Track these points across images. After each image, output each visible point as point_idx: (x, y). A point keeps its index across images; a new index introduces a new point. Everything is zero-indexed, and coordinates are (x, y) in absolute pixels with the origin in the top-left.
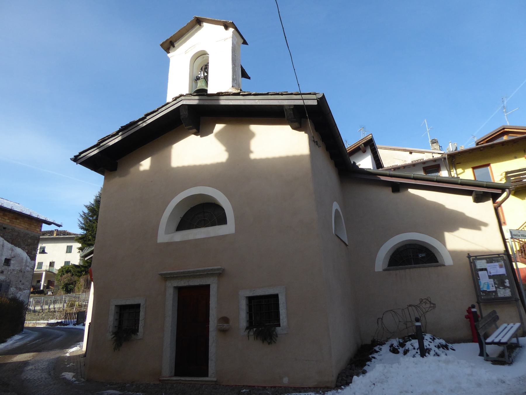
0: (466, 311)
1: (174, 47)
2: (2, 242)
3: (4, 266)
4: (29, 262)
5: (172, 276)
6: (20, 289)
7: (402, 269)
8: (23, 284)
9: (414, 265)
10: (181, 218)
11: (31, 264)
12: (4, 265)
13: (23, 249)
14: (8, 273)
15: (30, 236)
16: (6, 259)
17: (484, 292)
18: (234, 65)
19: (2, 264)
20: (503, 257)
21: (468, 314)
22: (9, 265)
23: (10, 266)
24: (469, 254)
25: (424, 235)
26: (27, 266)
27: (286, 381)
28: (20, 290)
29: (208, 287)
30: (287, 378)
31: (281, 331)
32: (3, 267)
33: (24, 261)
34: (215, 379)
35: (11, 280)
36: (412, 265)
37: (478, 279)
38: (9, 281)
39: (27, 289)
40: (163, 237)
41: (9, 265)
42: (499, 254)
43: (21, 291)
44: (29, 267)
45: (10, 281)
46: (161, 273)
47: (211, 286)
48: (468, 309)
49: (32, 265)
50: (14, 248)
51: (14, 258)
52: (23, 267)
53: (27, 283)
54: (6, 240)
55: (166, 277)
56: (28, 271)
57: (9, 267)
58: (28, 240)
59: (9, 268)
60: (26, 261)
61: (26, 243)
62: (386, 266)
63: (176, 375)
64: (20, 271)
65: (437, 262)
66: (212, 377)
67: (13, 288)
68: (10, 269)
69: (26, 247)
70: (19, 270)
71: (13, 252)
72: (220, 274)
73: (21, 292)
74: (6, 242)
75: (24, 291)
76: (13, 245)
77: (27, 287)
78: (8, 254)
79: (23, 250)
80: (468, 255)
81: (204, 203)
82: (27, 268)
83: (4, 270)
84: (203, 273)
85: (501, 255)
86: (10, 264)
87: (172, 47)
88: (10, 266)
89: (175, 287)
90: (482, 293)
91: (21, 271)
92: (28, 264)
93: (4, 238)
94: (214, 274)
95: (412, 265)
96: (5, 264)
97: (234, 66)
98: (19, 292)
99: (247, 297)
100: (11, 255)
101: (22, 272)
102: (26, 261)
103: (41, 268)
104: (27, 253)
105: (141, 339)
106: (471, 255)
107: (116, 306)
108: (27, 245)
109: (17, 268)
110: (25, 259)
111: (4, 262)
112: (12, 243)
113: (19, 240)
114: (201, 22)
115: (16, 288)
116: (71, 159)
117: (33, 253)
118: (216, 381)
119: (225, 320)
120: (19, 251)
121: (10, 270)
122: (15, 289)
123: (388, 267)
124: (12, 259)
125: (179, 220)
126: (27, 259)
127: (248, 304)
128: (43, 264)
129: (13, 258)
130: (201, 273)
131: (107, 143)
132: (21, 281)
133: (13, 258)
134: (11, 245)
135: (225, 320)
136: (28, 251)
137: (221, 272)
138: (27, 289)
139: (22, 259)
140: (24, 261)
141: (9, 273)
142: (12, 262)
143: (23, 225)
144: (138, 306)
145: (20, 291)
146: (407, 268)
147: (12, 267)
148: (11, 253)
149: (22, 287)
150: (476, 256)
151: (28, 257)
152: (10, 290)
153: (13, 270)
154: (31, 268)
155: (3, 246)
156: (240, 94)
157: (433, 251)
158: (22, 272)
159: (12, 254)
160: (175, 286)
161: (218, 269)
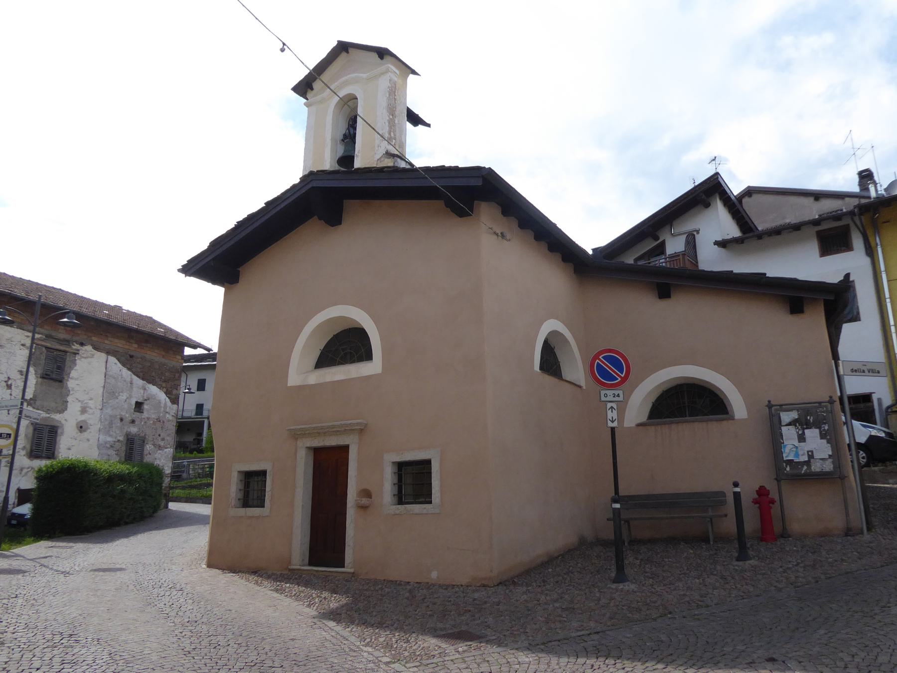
0: (755, 492)
1: (312, 89)
2: (130, 377)
3: (135, 413)
4: (170, 407)
5: (303, 433)
6: (160, 447)
7: (702, 421)
8: (163, 439)
9: (690, 416)
10: (320, 350)
11: (172, 409)
12: (135, 411)
13: (160, 387)
14: (141, 423)
15: (168, 368)
16: (137, 403)
17: (790, 462)
18: (392, 115)
19: (133, 410)
20: (826, 406)
21: (757, 497)
22: (141, 411)
23: (142, 412)
24: (769, 402)
25: (696, 367)
26: (167, 413)
27: (434, 575)
28: (160, 448)
29: (345, 449)
30: (436, 572)
31: (433, 509)
32: (134, 414)
33: (162, 405)
34: (352, 570)
35: (147, 434)
36: (686, 417)
37: (780, 441)
38: (143, 435)
39: (169, 446)
40: (294, 379)
41: (141, 411)
42: (820, 403)
43: (161, 450)
44: (169, 414)
45: (145, 435)
46: (289, 428)
47: (350, 447)
48: (759, 489)
49: (174, 411)
50: (146, 386)
51: (148, 401)
52: (162, 415)
53: (168, 438)
54: (134, 373)
55: (296, 435)
56: (169, 421)
57: (142, 414)
58: (166, 374)
59: (142, 415)
60: (165, 405)
61: (163, 378)
62: (644, 418)
63: (310, 564)
64: (157, 420)
65: (727, 413)
66: (348, 569)
67: (150, 446)
68: (143, 417)
69: (164, 385)
70: (156, 418)
71: (146, 392)
72: (362, 431)
73: (160, 451)
74: (135, 377)
75: (166, 450)
76: (145, 382)
77: (169, 444)
78: (140, 395)
79: (160, 388)
80: (767, 403)
81: (349, 328)
82: (168, 416)
83: (135, 419)
84: (340, 429)
85: (823, 404)
86: (143, 410)
87: (309, 90)
88: (142, 412)
89: (309, 448)
90: (784, 464)
91: (159, 420)
92: (168, 410)
93: (132, 372)
94: (353, 430)
95: (686, 418)
96: (137, 409)
97: (391, 117)
98: (159, 452)
99: (394, 463)
100: (143, 397)
101: (160, 421)
102: (165, 405)
103: (202, 414)
104: (166, 393)
105: (267, 516)
106: (773, 403)
107: (239, 472)
108: (165, 381)
109: (153, 416)
110: (163, 402)
111: (134, 406)
112: (143, 379)
113: (153, 374)
114: (349, 48)
115: (154, 445)
116: (179, 270)
117: (174, 393)
118: (354, 573)
119: (366, 493)
120: (153, 389)
121: (144, 418)
122: (153, 447)
123: (647, 419)
124: (145, 402)
125: (318, 353)
126: (165, 401)
127: (397, 471)
128: (205, 407)
129: (146, 400)
130: (338, 429)
131: (306, 185)
132: (159, 435)
133: (146, 400)
134: (141, 381)
135: (366, 493)
136: (167, 390)
137: (363, 428)
138: (169, 446)
139: (160, 402)
140: (162, 405)
141: (142, 423)
142: (145, 407)
143: (156, 351)
144: (263, 473)
145: (159, 449)
146: (672, 423)
147: (145, 415)
148: (144, 393)
149: (162, 443)
150: (781, 406)
151: (168, 400)
152: (145, 448)
153: (148, 418)
154: (173, 416)
155: (131, 383)
156: (384, 170)
157: (718, 393)
158: (160, 421)
159: (145, 395)
160: (308, 446)
161: (358, 424)
